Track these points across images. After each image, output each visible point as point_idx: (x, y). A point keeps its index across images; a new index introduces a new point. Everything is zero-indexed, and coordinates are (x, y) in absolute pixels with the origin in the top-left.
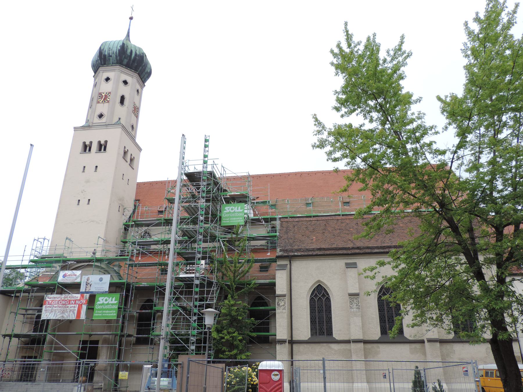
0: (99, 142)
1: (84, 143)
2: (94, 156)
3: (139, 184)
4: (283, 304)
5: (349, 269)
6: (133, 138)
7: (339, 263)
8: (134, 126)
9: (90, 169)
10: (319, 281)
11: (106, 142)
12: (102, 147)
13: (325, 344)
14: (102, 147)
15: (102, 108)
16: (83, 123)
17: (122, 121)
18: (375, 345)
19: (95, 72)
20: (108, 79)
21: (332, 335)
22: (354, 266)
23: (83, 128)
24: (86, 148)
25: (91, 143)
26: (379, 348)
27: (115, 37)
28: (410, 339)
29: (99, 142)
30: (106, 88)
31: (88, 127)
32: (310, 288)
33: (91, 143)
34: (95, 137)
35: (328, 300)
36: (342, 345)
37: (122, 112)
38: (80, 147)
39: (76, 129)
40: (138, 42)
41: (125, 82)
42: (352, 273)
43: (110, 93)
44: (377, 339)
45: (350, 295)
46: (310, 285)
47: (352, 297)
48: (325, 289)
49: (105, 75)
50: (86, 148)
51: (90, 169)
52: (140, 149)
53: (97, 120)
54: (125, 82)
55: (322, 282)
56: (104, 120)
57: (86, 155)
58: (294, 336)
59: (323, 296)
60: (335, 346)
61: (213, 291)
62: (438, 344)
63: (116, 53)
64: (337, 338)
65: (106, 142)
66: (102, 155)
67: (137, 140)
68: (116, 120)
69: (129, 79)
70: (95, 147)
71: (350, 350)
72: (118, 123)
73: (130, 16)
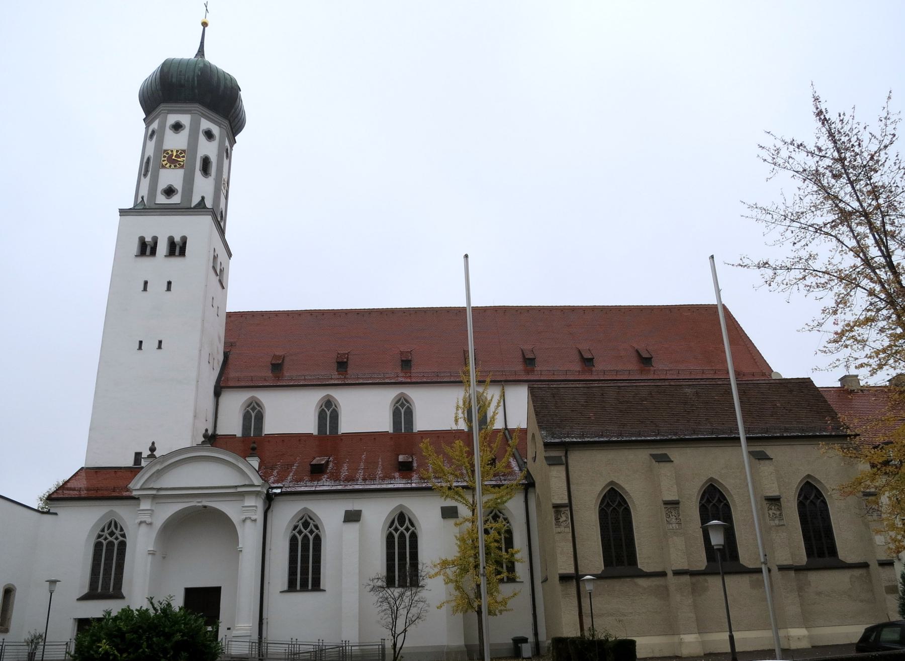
2: (161, 266)
3: (230, 315)
4: (564, 518)
5: (552, 468)
7: (642, 455)
9: (157, 287)
10: (809, 476)
13: (628, 579)
14: (177, 249)
16: (131, 205)
17: (209, 204)
20: (177, 127)
22: (664, 459)
24: (147, 249)
28: (751, 567)
30: (175, 142)
31: (141, 208)
32: (599, 494)
34: (162, 228)
35: (627, 511)
37: (203, 187)
38: (135, 247)
39: (123, 212)
40: (219, 58)
41: (209, 135)
42: (665, 469)
44: (703, 568)
45: (666, 503)
46: (599, 488)
47: (669, 506)
48: (816, 488)
49: (172, 119)
50: (147, 249)
51: (157, 287)
52: (230, 255)
53: (161, 199)
55: (716, 481)
56: (176, 199)
57: (147, 261)
58: (579, 568)
59: (620, 505)
60: (643, 582)
62: (792, 573)
63: (193, 78)
64: (645, 570)
65: (184, 240)
66: (176, 261)
68: (195, 200)
69: (216, 130)
70: (162, 248)
71: (666, 588)
72: (201, 205)
73: (201, 19)
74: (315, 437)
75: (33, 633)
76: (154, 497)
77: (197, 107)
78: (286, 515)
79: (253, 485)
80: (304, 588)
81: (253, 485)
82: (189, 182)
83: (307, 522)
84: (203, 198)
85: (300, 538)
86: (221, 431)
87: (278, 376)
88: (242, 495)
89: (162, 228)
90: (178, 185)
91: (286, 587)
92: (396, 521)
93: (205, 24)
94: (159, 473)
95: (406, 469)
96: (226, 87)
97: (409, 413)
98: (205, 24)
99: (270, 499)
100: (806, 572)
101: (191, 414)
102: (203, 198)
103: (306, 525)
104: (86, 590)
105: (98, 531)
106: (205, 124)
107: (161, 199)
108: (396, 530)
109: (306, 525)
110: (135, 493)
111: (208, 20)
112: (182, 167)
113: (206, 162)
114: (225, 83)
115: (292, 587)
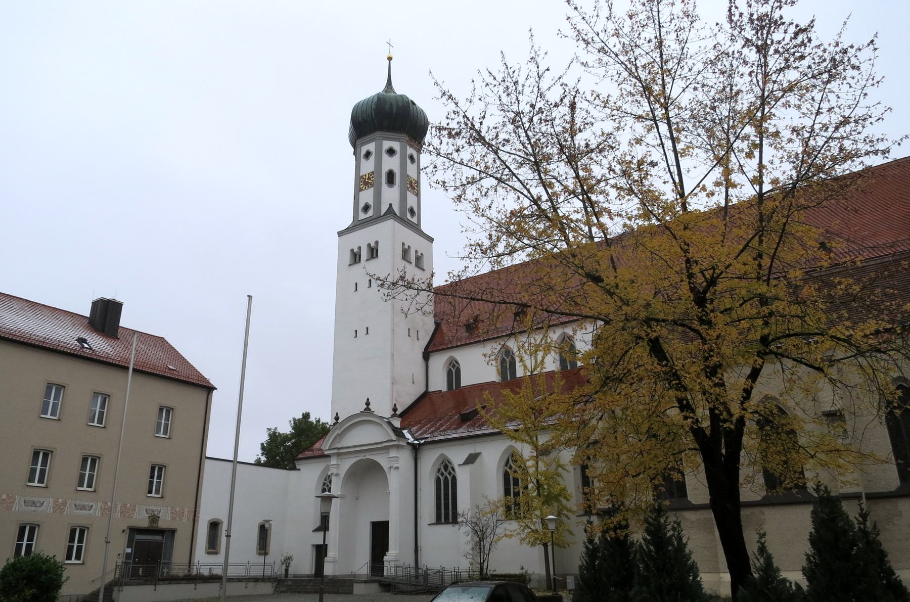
0: (369, 245)
1: (352, 250)
6: (416, 228)
8: (416, 210)
11: (377, 243)
12: (373, 252)
15: (367, 196)
16: (348, 221)
17: (396, 209)
18: (756, 510)
19: (354, 145)
21: (685, 495)
23: (349, 230)
24: (356, 257)
25: (360, 248)
26: (763, 513)
27: (373, 88)
29: (369, 245)
31: (357, 225)
33: (360, 248)
34: (363, 239)
36: (702, 512)
38: (348, 258)
39: (340, 234)
41: (391, 152)
43: (373, 172)
44: (759, 498)
54: (391, 152)
56: (370, 213)
57: (358, 268)
61: (758, 560)
64: (693, 502)
66: (373, 262)
67: (424, 228)
68: (384, 209)
73: (387, 55)
74: (498, 383)
75: (285, 555)
76: (339, 455)
77: (378, 134)
78: (430, 460)
79: (392, 441)
80: (447, 522)
81: (392, 441)
82: (378, 196)
83: (446, 466)
84: (391, 205)
85: (442, 479)
86: (431, 389)
87: (473, 333)
88: (387, 448)
89: (363, 239)
90: (371, 203)
91: (434, 520)
92: (510, 461)
93: (390, 59)
94: (341, 436)
95: (467, 418)
96: (398, 108)
97: (458, 371)
98: (390, 59)
99: (416, 449)
100: (894, 500)
101: (388, 381)
102: (391, 205)
103: (446, 467)
104: (318, 524)
105: (322, 481)
106: (387, 144)
107: (362, 216)
108: (511, 468)
109: (446, 467)
110: (326, 453)
111: (393, 55)
112: (372, 186)
113: (391, 176)
114: (398, 105)
115: (438, 521)
